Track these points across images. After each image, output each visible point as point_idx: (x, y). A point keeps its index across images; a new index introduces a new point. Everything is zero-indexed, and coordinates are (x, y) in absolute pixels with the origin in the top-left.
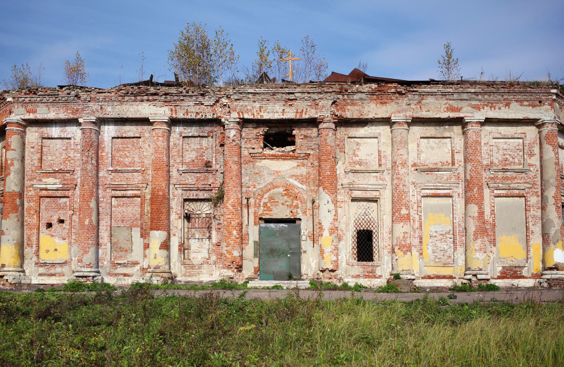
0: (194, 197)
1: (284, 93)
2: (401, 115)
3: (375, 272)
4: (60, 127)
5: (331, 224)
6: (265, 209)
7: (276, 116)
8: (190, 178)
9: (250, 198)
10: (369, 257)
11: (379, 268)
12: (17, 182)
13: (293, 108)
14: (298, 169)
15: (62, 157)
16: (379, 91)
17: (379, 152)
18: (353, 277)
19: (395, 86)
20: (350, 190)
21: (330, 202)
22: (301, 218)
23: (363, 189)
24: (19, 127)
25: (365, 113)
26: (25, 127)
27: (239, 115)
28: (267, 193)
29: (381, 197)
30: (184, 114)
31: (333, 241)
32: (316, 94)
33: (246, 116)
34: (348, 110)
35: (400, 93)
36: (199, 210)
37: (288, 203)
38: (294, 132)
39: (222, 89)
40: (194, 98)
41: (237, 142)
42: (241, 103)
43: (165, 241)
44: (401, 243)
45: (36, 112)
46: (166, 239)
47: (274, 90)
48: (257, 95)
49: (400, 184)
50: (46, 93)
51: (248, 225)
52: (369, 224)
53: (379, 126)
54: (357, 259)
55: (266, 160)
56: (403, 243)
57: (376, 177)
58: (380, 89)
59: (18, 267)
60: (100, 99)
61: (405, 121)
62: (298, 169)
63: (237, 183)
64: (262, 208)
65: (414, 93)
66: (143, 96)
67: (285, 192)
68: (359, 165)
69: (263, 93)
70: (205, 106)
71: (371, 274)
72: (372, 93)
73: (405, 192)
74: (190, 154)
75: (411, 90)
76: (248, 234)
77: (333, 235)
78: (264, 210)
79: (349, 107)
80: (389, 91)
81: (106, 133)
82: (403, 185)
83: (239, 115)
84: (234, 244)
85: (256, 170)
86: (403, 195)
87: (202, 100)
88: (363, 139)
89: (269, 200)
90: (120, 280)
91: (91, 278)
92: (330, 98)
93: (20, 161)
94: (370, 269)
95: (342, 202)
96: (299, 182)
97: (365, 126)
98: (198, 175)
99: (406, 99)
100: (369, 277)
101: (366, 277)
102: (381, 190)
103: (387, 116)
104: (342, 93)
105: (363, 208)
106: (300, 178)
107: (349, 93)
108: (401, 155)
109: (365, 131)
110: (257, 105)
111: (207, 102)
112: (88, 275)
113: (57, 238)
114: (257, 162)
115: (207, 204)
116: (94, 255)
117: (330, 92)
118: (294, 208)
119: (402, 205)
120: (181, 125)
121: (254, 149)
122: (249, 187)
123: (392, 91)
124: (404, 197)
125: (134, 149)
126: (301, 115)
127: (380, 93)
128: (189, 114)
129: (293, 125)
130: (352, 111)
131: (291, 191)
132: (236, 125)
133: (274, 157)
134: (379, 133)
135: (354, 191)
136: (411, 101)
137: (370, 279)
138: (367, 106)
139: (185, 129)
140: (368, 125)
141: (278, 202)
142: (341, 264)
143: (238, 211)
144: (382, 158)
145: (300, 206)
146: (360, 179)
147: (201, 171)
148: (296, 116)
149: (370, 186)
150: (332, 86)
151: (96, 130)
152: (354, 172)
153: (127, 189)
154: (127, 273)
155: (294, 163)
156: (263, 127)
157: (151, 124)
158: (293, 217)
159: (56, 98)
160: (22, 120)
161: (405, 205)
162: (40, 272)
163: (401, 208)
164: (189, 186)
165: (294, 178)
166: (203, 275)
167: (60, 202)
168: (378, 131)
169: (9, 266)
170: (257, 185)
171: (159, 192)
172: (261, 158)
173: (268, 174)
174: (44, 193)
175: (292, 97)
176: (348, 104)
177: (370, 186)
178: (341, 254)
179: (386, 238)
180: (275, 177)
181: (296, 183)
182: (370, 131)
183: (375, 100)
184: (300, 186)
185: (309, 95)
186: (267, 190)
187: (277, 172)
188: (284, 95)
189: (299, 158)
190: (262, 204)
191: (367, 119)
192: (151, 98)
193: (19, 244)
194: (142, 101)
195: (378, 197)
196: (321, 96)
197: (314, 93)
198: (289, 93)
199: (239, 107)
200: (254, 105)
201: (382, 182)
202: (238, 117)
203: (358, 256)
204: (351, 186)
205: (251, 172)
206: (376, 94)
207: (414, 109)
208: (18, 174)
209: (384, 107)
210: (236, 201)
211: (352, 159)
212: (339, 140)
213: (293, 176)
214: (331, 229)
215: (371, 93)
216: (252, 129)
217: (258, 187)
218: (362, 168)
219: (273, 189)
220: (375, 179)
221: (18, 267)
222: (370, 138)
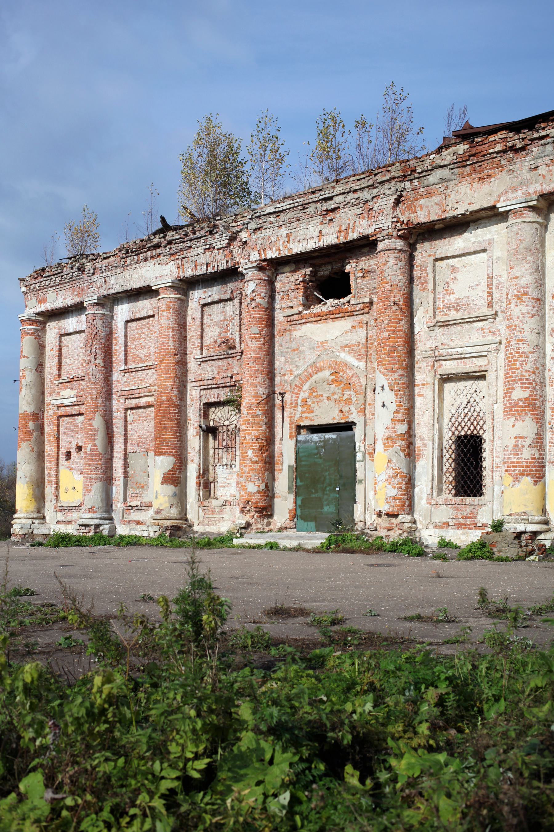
0: (216, 400)
1: (318, 201)
2: (519, 193)
3: (476, 518)
4: (77, 316)
5: (387, 428)
6: (305, 409)
7: (310, 246)
8: (210, 369)
9: (285, 393)
10: (475, 487)
11: (483, 508)
12: (29, 400)
13: (334, 225)
14: (354, 334)
15: (80, 359)
16: (474, 155)
17: (490, 278)
18: (436, 526)
19: (503, 136)
20: (437, 361)
21: (386, 387)
22: (355, 421)
23: (457, 356)
24: (32, 325)
25: (450, 206)
26: (44, 323)
27: (260, 255)
28: (307, 381)
29: (490, 369)
30: (192, 270)
31: (390, 461)
32: (367, 190)
33: (271, 254)
34: (421, 207)
35: (513, 149)
36: (227, 420)
37: (336, 397)
38: (348, 268)
39: (239, 217)
40: (202, 240)
41: (258, 301)
42: (263, 233)
43: (169, 471)
44: (509, 458)
45: (46, 300)
46: (173, 468)
47: (302, 199)
48: (282, 215)
49: (512, 338)
50: (52, 273)
51: (281, 440)
52: (475, 423)
53: (490, 225)
54: (453, 492)
55: (309, 324)
56: (514, 458)
57: (483, 329)
58: (474, 151)
59: (32, 512)
60: (103, 268)
61: (524, 205)
62: (354, 334)
63: (257, 370)
64: (300, 408)
65: (542, 142)
66: (146, 252)
67: (333, 377)
68: (455, 310)
69: (289, 209)
70: (218, 249)
71: (468, 522)
72: (461, 163)
73: (523, 353)
74: (212, 331)
75: (536, 135)
76: (282, 454)
77: (390, 450)
78: (303, 412)
79: (422, 201)
80: (491, 151)
81: (119, 315)
82: (518, 341)
83: (260, 255)
84: (249, 473)
85: (294, 343)
86: (517, 360)
87: (212, 242)
88: (463, 258)
89: (310, 394)
90: (133, 529)
91: (93, 527)
92: (390, 192)
93: (34, 371)
94: (467, 511)
95: (423, 385)
96: (354, 356)
97: (465, 231)
98: (220, 363)
99: (527, 159)
100: (464, 526)
101: (460, 526)
102: (490, 355)
103: (491, 204)
104: (408, 178)
105: (465, 392)
106: (356, 348)
107: (420, 173)
108: (516, 277)
109: (464, 241)
110: (284, 231)
111: (219, 243)
112: (88, 523)
113: (75, 471)
114: (295, 330)
115: (226, 409)
116: (99, 495)
117: (388, 181)
118: (345, 403)
119: (515, 380)
120: (200, 287)
121: (292, 307)
122: (284, 375)
123: (496, 150)
124: (518, 365)
125: (149, 333)
126: (346, 235)
127: (475, 160)
128: (199, 268)
129: (348, 255)
130: (427, 207)
131: (341, 374)
132: (256, 272)
133: (320, 318)
134: (489, 240)
135: (443, 363)
136: (540, 161)
137: (467, 530)
138: (454, 192)
139: (205, 292)
140: (471, 228)
141: (322, 396)
142: (419, 502)
143: (257, 416)
144: (494, 290)
145: (354, 399)
146: (454, 337)
147: (222, 357)
148: (338, 238)
149: (469, 350)
150: (390, 168)
151: (104, 315)
152: (443, 326)
153: (140, 395)
154: (141, 519)
155: (345, 324)
156: (304, 267)
157: (156, 293)
158: (343, 421)
159: (62, 276)
160: (36, 314)
161: (520, 380)
162: (58, 519)
163: (513, 388)
164: (206, 382)
165: (347, 349)
166: (224, 523)
167: (78, 421)
168: (489, 237)
169: (21, 512)
170: (294, 369)
171: (161, 396)
172: (300, 322)
173: (310, 349)
174: (62, 411)
175: (331, 205)
176: (421, 196)
177: (469, 350)
178: (419, 483)
179: (498, 450)
180: (319, 353)
181: (350, 359)
182: (473, 240)
183: (469, 175)
184: (355, 363)
185: (356, 196)
186: (307, 377)
187: (322, 343)
188: (319, 205)
189: (355, 313)
190: (299, 401)
191: (455, 217)
192: (154, 253)
193: (33, 482)
194: (146, 260)
195: (483, 369)
196: (375, 192)
197: (362, 189)
198: (326, 199)
199: (260, 242)
200: (280, 233)
201: (493, 338)
202: (258, 258)
203: (455, 487)
204: (437, 353)
205: (288, 348)
206: (469, 162)
207: (544, 176)
208: (31, 388)
209: (487, 185)
210: (253, 401)
211: (443, 301)
212: (419, 268)
213: (346, 346)
214: (387, 439)
215: (459, 164)
216: (290, 274)
217: (296, 373)
218: (460, 315)
219: (316, 373)
220: (481, 332)
221: (32, 512)
222: (474, 253)
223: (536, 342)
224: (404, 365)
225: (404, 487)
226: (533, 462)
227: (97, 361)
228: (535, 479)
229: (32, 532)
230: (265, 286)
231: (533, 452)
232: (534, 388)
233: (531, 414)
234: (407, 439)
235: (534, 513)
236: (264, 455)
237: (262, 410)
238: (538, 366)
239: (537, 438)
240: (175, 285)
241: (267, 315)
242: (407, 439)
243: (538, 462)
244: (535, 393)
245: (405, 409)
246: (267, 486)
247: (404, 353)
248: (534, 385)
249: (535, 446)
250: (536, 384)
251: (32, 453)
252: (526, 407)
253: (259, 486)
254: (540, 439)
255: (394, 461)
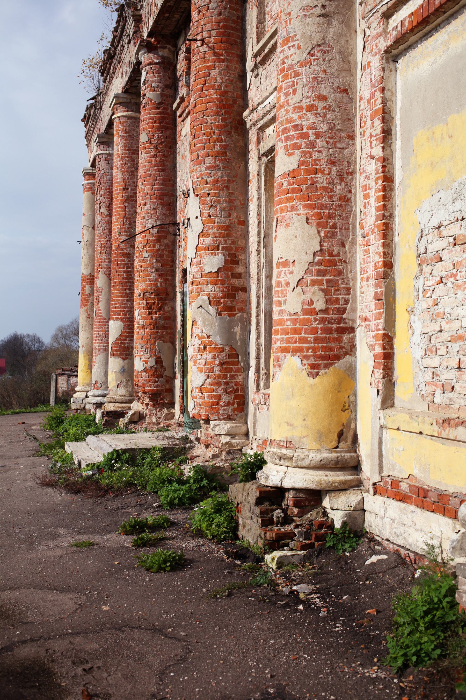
46: (121, 336)
223: (317, 38)
224: (217, 148)
225: (217, 370)
226: (309, 321)
227: (102, 210)
228: (312, 361)
229: (84, 408)
230: (158, 72)
231: (308, 297)
232: (312, 145)
233: (305, 206)
234: (223, 282)
235: (309, 443)
236: (154, 316)
237: (150, 251)
238: (324, 92)
239: (320, 263)
240: (121, 100)
241: (160, 113)
242: (223, 282)
243: (323, 320)
244: (316, 155)
245: (219, 228)
246: (159, 361)
247: (217, 127)
248: (312, 137)
249: (313, 283)
250: (318, 135)
251: (88, 319)
252: (293, 191)
253: (146, 362)
254: (332, 263)
255: (199, 323)
